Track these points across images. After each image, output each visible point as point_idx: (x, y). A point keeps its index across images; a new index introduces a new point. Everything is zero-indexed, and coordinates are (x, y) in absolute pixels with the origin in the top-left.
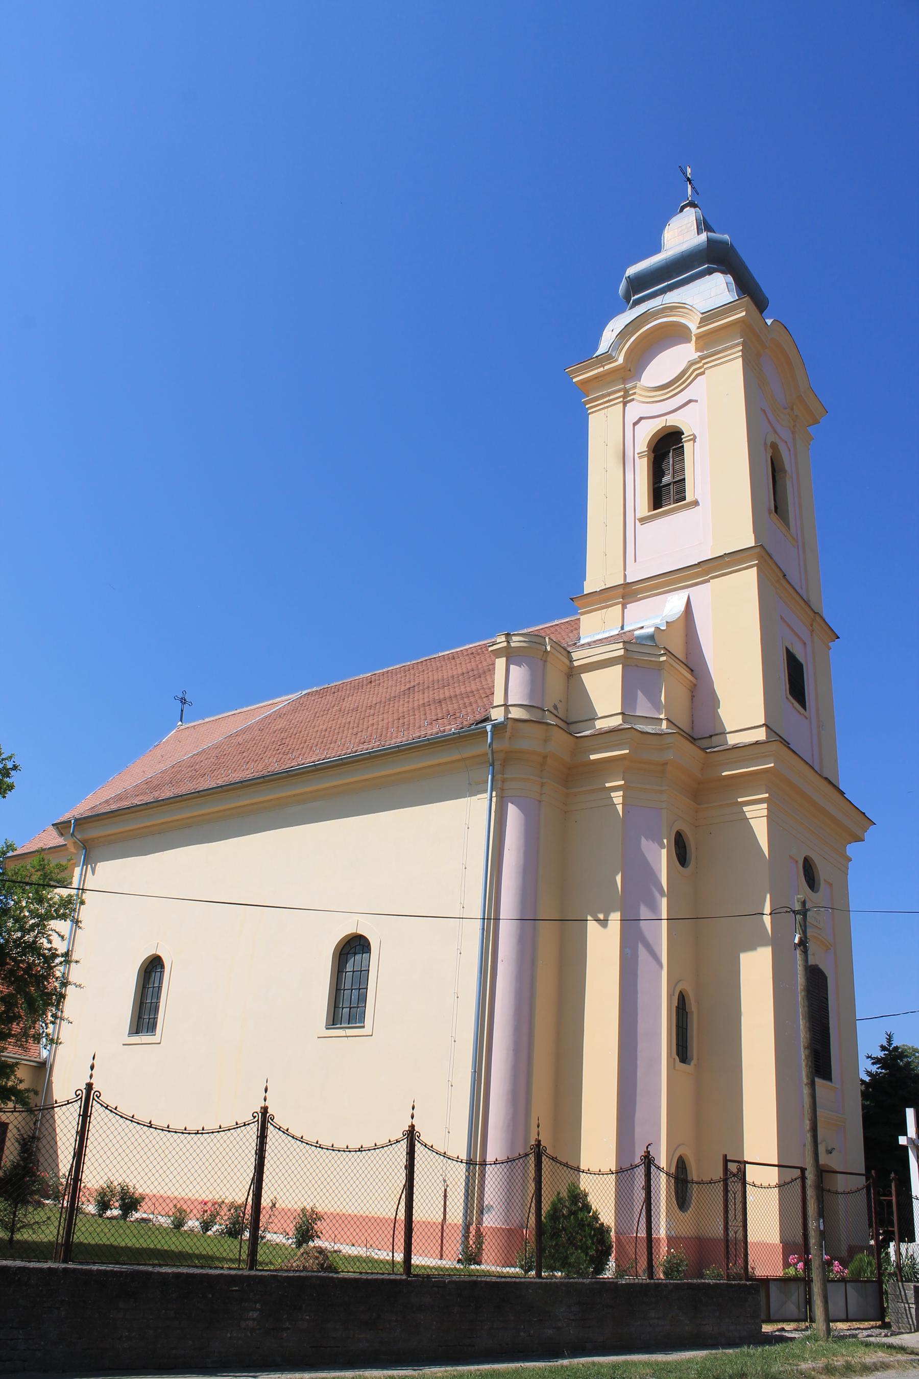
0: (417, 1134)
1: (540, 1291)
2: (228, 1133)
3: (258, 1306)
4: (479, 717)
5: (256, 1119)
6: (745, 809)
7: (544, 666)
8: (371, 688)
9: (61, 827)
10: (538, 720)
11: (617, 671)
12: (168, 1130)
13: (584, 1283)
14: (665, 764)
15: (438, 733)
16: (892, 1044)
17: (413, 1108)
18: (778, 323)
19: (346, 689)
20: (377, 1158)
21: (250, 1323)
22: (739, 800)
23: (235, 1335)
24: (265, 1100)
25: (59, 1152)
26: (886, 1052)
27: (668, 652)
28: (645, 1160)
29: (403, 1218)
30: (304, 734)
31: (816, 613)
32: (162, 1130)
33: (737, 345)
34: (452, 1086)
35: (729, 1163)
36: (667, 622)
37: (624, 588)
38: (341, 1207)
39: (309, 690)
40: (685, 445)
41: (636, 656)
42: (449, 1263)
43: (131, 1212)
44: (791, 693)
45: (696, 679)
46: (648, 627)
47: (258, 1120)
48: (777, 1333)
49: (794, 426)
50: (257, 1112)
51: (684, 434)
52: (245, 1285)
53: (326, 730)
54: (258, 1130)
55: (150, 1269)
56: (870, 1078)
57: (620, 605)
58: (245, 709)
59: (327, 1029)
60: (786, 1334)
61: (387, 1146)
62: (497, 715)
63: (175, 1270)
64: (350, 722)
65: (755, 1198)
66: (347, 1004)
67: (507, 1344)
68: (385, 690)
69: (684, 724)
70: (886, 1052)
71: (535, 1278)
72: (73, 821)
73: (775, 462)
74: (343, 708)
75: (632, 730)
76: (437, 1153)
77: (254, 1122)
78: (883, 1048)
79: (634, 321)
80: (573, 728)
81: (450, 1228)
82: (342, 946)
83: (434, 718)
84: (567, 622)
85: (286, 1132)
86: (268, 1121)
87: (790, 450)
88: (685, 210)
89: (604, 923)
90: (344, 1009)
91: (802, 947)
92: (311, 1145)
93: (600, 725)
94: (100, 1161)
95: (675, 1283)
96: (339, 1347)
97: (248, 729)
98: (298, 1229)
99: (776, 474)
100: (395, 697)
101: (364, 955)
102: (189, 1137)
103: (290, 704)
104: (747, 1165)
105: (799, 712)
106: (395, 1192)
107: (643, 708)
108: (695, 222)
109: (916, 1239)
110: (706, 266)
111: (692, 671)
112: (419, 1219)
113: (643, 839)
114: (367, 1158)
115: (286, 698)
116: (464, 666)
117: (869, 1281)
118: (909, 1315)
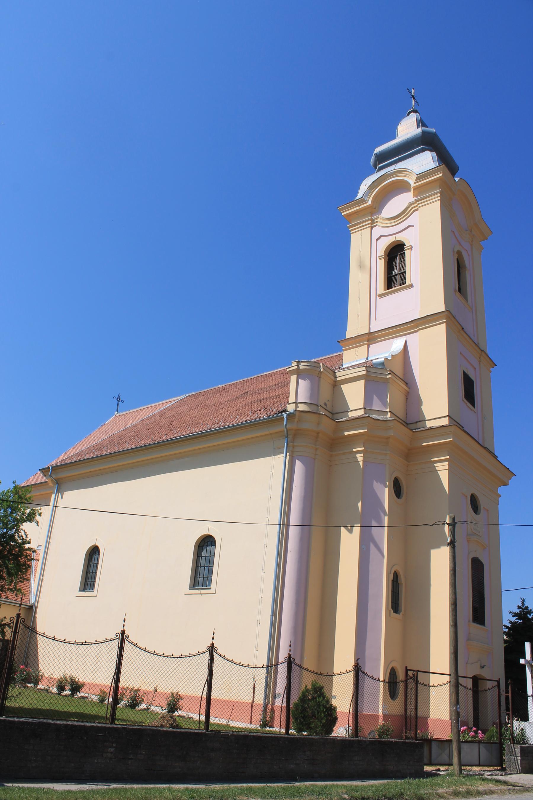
0: (216, 648)
1: (287, 742)
2: (101, 645)
3: (114, 745)
4: (280, 410)
5: (118, 637)
6: (435, 465)
7: (319, 381)
8: (224, 393)
9: (44, 471)
10: (314, 411)
11: (362, 383)
12: (65, 642)
13: (314, 738)
14: (388, 438)
15: (256, 419)
16: (524, 605)
17: (214, 634)
18: (462, 180)
19: (210, 394)
20: (191, 662)
21: (109, 755)
22: (432, 460)
23: (100, 761)
24: (124, 626)
25: (39, 658)
26: (521, 610)
27: (392, 373)
28: (356, 668)
29: (205, 697)
30: (183, 419)
31: (482, 351)
32: (61, 642)
33: (437, 193)
34: (259, 624)
35: (408, 671)
36: (392, 355)
37: (369, 335)
38: (195, 692)
39: (190, 394)
40: (406, 251)
41: (373, 375)
42: (255, 726)
43: (77, 693)
44: (465, 397)
45: (409, 389)
46: (381, 358)
47: (119, 638)
48: (434, 772)
49: (472, 241)
50: (118, 633)
51: (405, 245)
52: (107, 732)
53: (196, 417)
54: (119, 643)
55: (50, 721)
56: (511, 625)
57: (367, 345)
58: (154, 405)
59: (190, 589)
60: (440, 773)
61: (197, 655)
62: (291, 408)
63: (65, 722)
64: (209, 412)
65: (435, 693)
66: (202, 575)
67: (266, 773)
68: (231, 394)
69: (401, 414)
70: (521, 610)
71: (284, 735)
72: (51, 468)
73: (459, 261)
74: (207, 404)
75: (369, 418)
76: (227, 660)
77: (116, 639)
78: (519, 607)
79: (378, 180)
80: (336, 416)
81: (256, 706)
82: (200, 542)
83: (256, 410)
84: (337, 355)
85: (136, 645)
86: (125, 639)
87: (469, 255)
88: (411, 114)
89: (351, 531)
90: (200, 578)
91: (452, 545)
92: (151, 653)
93: (351, 415)
94: (62, 664)
95: (371, 740)
96: (162, 770)
97: (154, 416)
98: (169, 704)
99: (460, 269)
100: (236, 398)
101: (212, 547)
102: (77, 646)
103: (178, 402)
104: (418, 673)
105: (470, 409)
106: (203, 680)
107: (377, 405)
108: (416, 121)
109: (529, 720)
110: (421, 147)
111: (407, 384)
112: (215, 698)
113: (375, 482)
114: (184, 661)
115: (177, 398)
116: (277, 380)
117: (495, 743)
118: (517, 764)
